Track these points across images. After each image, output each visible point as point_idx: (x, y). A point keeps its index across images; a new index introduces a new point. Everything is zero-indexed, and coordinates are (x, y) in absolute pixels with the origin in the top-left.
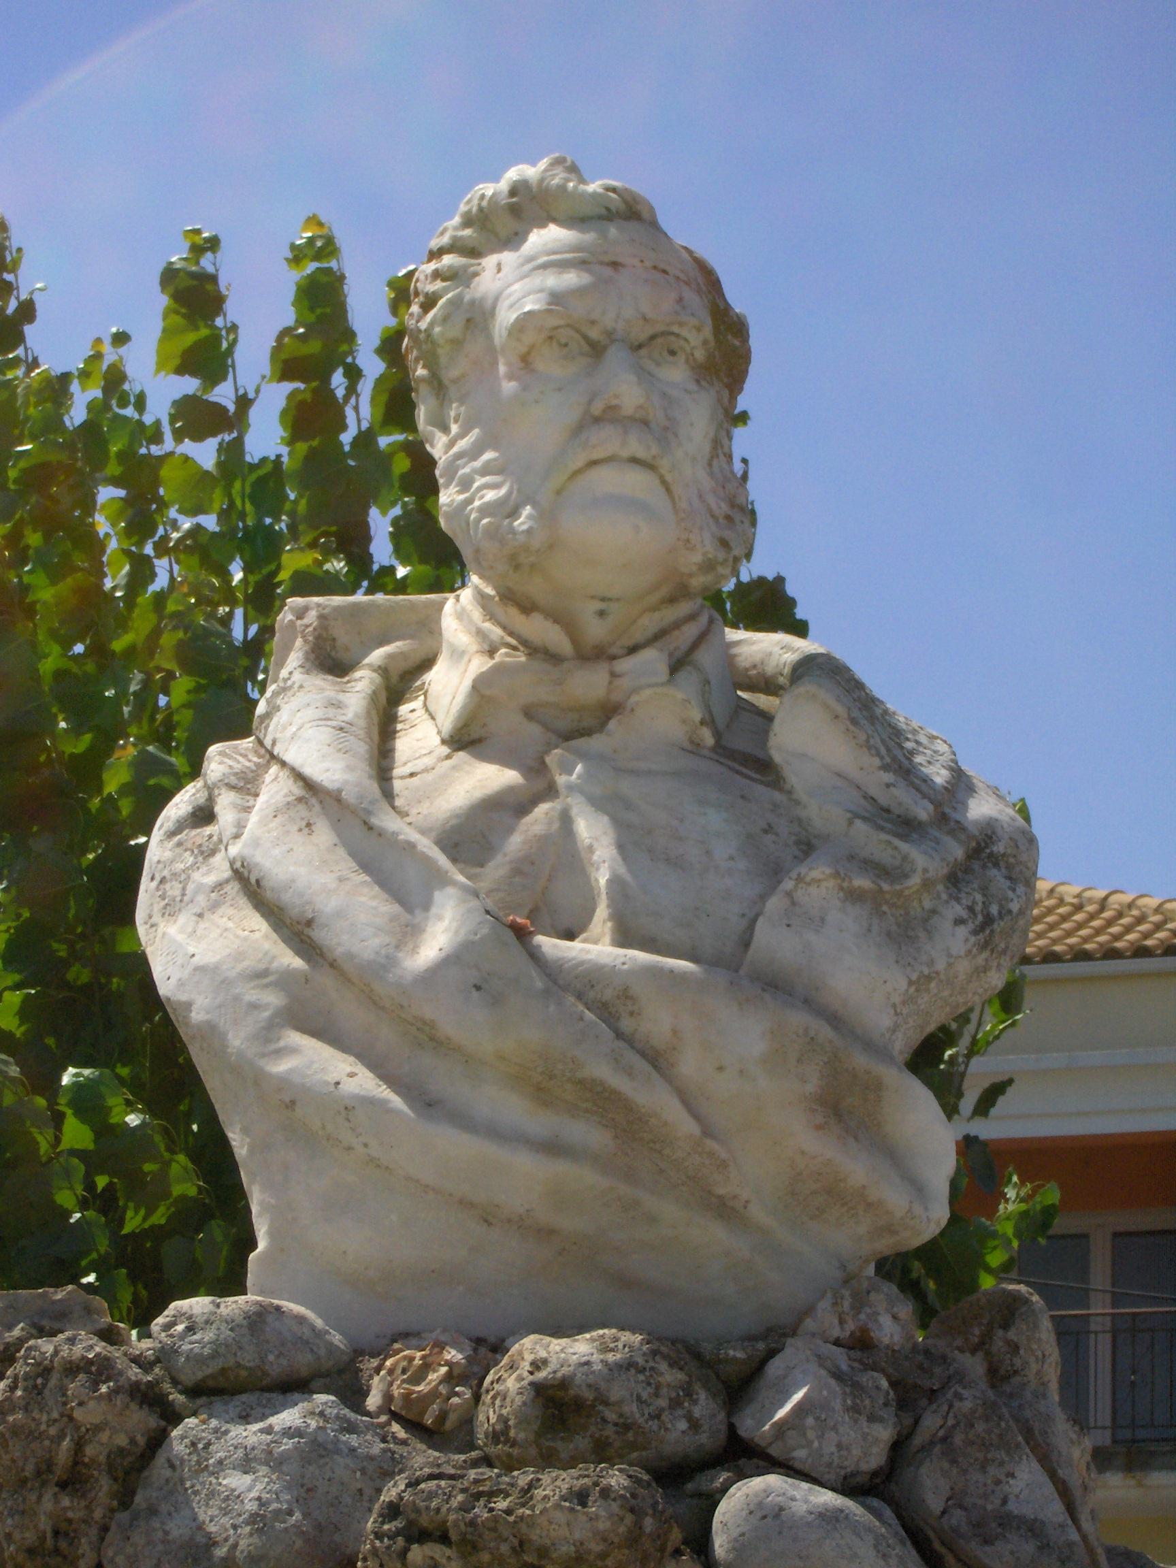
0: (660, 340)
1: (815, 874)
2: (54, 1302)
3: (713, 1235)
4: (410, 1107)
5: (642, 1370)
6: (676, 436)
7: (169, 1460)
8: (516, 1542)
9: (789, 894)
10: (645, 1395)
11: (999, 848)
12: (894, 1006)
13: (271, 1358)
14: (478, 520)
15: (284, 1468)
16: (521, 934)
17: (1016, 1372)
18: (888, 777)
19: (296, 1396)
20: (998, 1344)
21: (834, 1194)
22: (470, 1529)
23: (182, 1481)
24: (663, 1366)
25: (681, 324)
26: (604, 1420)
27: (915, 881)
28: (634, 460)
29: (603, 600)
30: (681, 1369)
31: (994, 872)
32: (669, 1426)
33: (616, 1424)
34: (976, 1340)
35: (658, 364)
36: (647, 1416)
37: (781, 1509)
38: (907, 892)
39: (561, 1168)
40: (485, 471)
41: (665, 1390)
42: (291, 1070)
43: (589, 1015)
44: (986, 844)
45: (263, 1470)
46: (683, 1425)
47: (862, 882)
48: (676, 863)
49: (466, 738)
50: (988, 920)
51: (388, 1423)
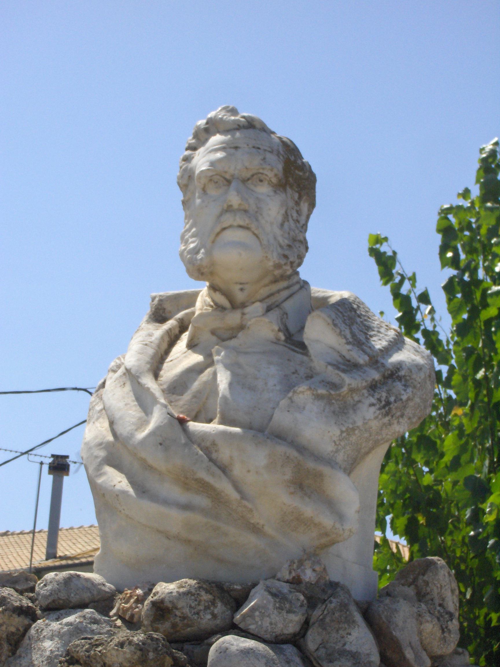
0: (255, 177)
1: (301, 389)
2: (14, 577)
3: (251, 540)
4: (135, 493)
5: (193, 595)
6: (261, 215)
7: (29, 637)
8: (102, 663)
9: (290, 398)
10: (193, 605)
11: (402, 373)
12: (335, 442)
13: (72, 595)
14: (187, 256)
15: (63, 638)
16: (182, 422)
17: (428, 593)
18: (349, 347)
19: (79, 610)
20: (420, 582)
21: (299, 521)
22: (87, 659)
23: (31, 644)
24: (203, 593)
25: (263, 169)
26: (176, 615)
27: (345, 389)
28: (240, 227)
29: (241, 284)
30: (211, 594)
31: (399, 383)
32: (202, 617)
33: (180, 617)
34: (411, 580)
35: (255, 186)
36: (192, 613)
37: (227, 649)
38: (342, 394)
39: (188, 515)
40: (193, 236)
41: (203, 602)
42: (103, 481)
43: (201, 452)
44: (396, 372)
45: (57, 639)
46: (209, 617)
47: (322, 391)
48: (252, 389)
49: (193, 345)
50: (388, 403)
51: (116, 620)
